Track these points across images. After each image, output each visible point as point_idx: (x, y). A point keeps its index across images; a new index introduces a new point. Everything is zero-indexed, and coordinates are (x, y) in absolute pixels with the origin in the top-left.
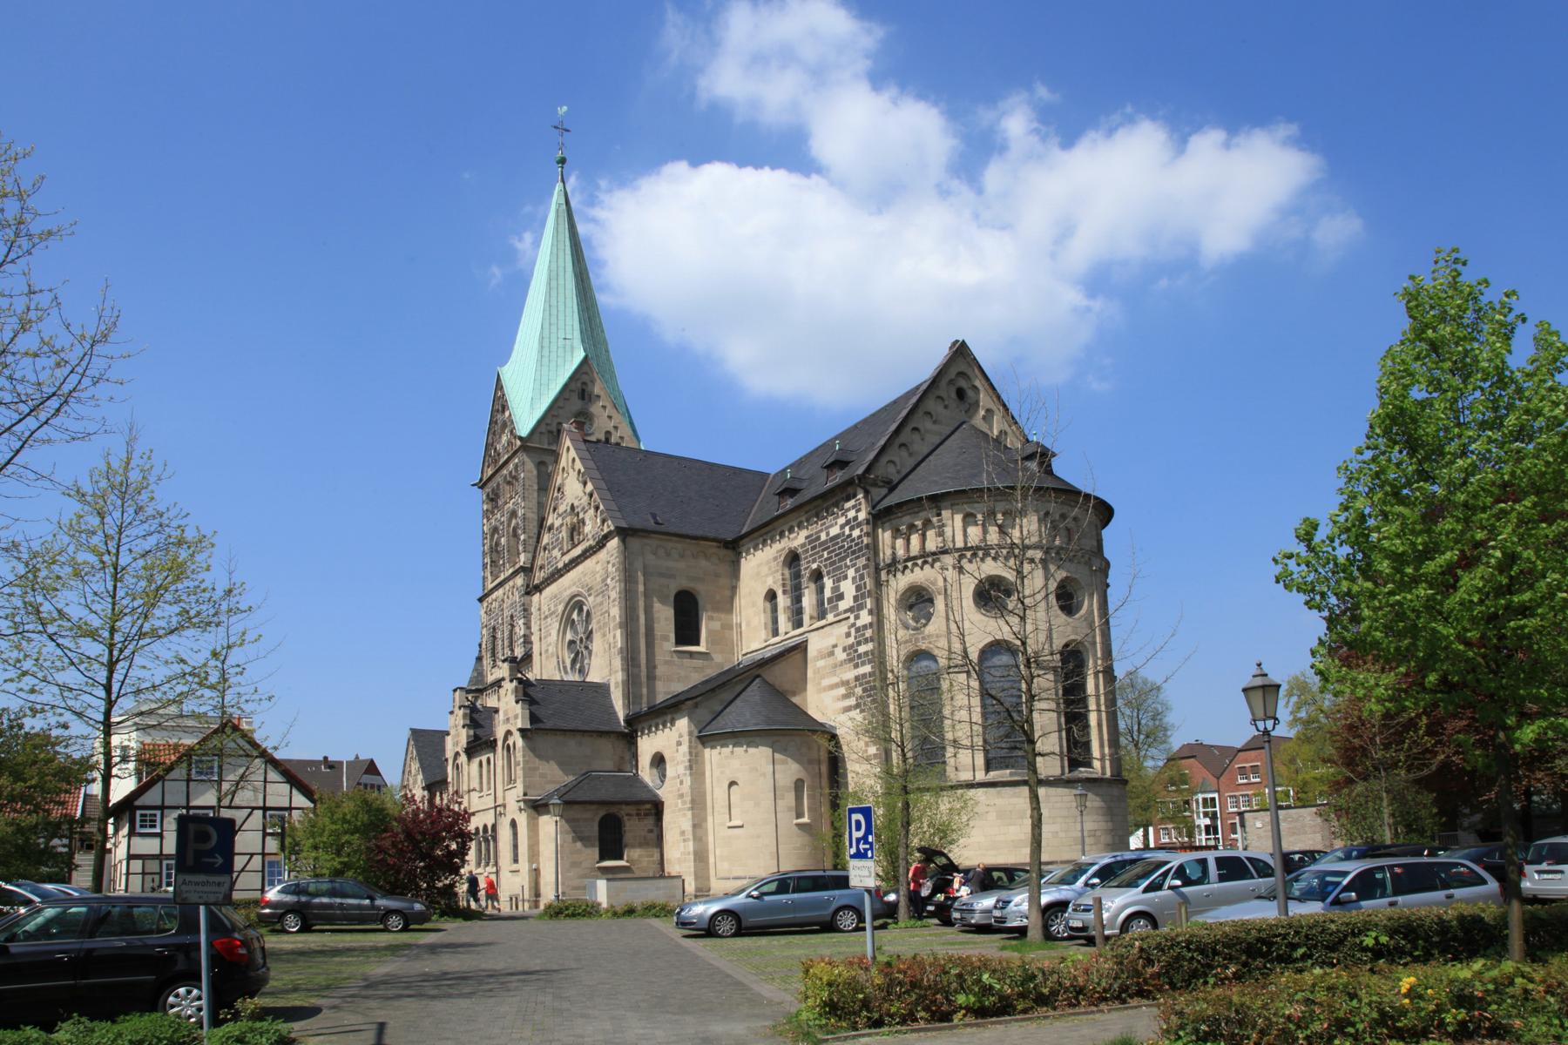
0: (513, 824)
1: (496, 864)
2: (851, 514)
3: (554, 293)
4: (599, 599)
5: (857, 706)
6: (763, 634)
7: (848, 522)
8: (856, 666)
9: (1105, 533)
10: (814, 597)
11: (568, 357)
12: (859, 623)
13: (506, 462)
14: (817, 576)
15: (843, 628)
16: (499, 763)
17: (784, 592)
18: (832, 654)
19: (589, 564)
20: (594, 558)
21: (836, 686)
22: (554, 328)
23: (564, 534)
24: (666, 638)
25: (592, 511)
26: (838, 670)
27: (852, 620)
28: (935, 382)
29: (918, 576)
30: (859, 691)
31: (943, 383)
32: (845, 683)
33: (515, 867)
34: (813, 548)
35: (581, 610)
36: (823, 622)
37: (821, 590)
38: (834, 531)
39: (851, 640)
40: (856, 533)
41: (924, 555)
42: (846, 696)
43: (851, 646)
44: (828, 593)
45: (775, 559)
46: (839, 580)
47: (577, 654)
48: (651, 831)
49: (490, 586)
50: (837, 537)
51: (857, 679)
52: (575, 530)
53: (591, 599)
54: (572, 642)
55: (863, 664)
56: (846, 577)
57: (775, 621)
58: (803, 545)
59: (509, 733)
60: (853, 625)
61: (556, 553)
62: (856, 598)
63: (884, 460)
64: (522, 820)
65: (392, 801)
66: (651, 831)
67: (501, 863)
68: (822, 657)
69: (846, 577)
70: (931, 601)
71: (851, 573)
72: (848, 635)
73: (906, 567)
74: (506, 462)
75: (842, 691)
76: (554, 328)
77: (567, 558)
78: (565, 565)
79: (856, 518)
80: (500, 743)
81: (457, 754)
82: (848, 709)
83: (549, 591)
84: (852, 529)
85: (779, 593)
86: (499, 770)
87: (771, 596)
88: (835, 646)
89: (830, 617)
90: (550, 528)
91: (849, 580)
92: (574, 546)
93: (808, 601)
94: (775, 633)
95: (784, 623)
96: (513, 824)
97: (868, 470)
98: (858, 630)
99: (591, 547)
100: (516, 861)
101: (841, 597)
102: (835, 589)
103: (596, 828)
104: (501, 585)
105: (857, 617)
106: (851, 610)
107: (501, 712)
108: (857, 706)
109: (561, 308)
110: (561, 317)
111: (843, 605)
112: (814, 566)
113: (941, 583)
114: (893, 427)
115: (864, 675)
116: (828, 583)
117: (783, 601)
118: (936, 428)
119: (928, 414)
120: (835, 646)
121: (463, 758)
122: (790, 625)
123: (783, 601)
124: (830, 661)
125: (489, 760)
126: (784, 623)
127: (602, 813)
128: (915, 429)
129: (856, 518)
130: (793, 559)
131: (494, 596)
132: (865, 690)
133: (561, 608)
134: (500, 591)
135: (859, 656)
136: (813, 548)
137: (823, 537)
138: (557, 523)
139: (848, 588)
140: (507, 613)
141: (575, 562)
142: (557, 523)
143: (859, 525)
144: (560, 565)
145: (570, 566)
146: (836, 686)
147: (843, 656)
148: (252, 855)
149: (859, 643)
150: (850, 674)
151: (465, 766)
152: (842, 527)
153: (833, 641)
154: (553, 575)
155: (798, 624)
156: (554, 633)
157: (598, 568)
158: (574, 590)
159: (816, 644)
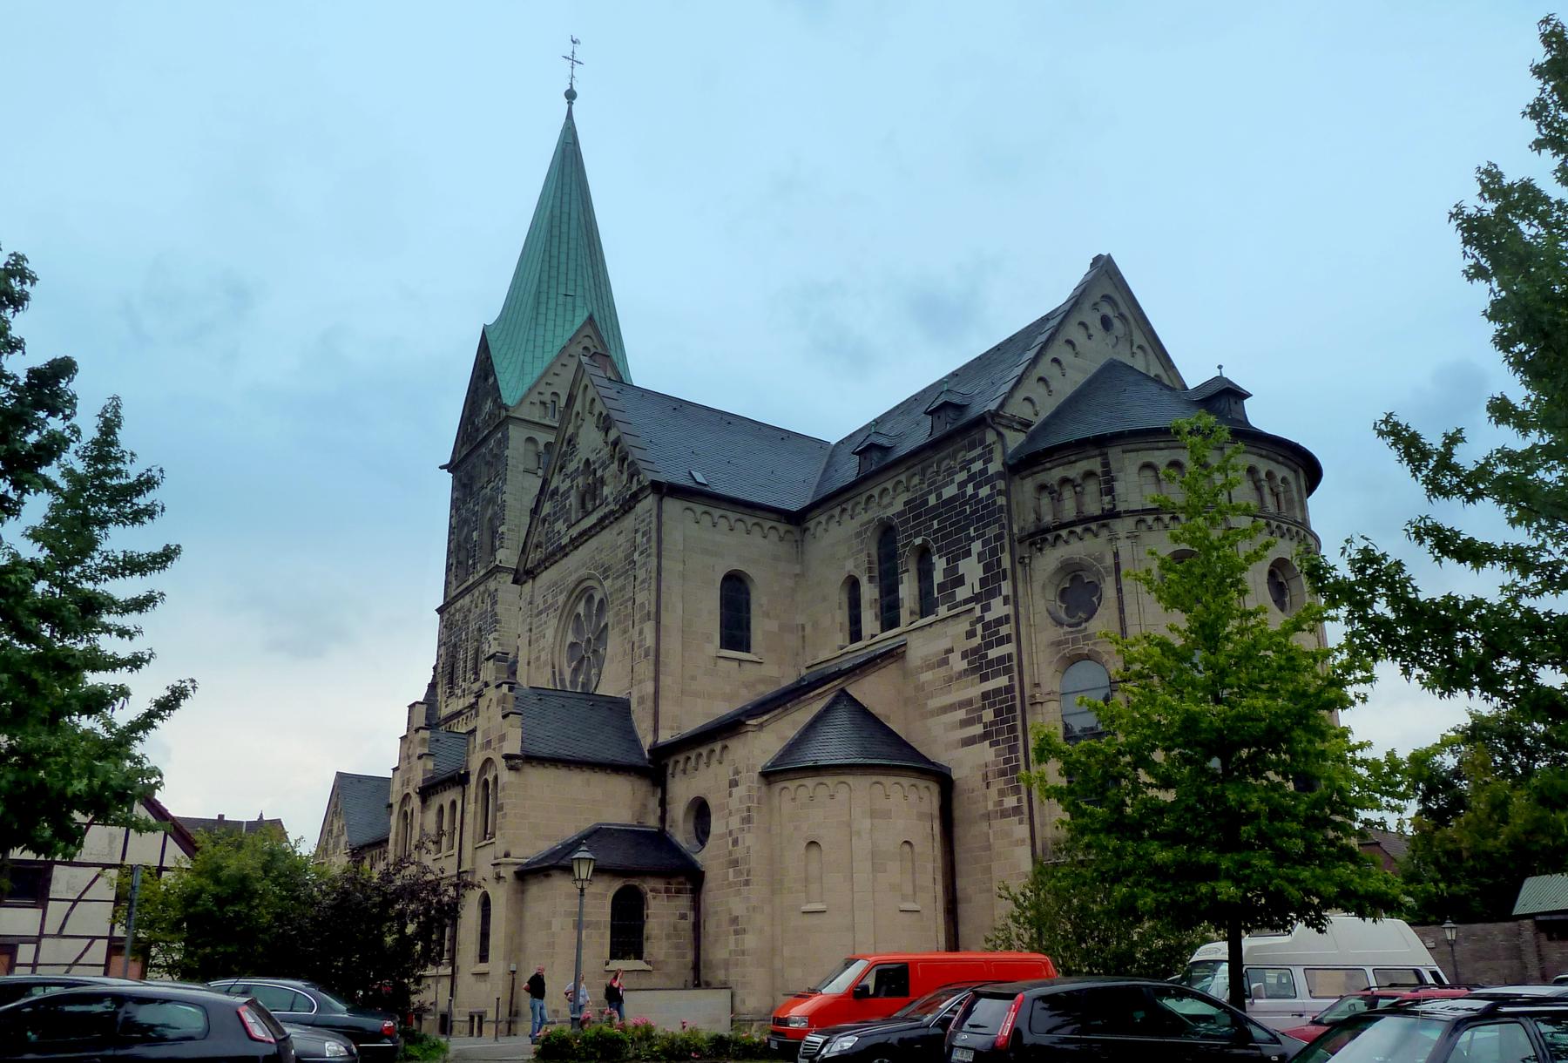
0: (486, 902)
1: (452, 962)
2: (977, 466)
3: (555, 241)
4: (620, 582)
5: (985, 736)
6: (841, 638)
7: (971, 478)
8: (984, 678)
9: (1313, 501)
10: (915, 584)
11: (569, 317)
12: (989, 617)
13: (485, 439)
14: (924, 554)
15: (963, 625)
16: (471, 808)
17: (871, 579)
18: (945, 662)
19: (607, 536)
20: (616, 528)
21: (952, 707)
22: (553, 283)
23: (573, 500)
24: (709, 639)
25: (615, 466)
26: (954, 686)
27: (978, 612)
28: (1076, 302)
29: (1077, 549)
30: (988, 715)
31: (1087, 305)
32: (967, 703)
33: (482, 967)
34: (916, 518)
35: (590, 599)
36: (931, 618)
37: (925, 574)
38: (949, 492)
39: (977, 641)
40: (984, 491)
41: (1083, 520)
42: (965, 723)
43: (975, 651)
44: (938, 577)
45: (858, 534)
46: (956, 559)
47: (581, 662)
48: (683, 917)
49: (454, 594)
50: (953, 499)
51: (985, 696)
52: (590, 494)
53: (607, 583)
54: (573, 645)
55: (996, 674)
56: (968, 554)
57: (855, 621)
58: (900, 514)
59: (488, 762)
60: (981, 619)
61: (560, 526)
62: (983, 582)
63: (1020, 394)
64: (500, 899)
65: (299, 867)
66: (683, 917)
67: (459, 960)
68: (930, 667)
69: (968, 554)
70: (1095, 588)
71: (977, 547)
72: (971, 634)
73: (1058, 537)
74: (485, 439)
75: (961, 714)
76: (553, 283)
77: (574, 532)
78: (572, 540)
79: (984, 471)
80: (473, 779)
81: (407, 797)
82: (969, 742)
83: (546, 577)
84: (977, 487)
85: (864, 581)
86: (469, 818)
87: (853, 584)
88: (951, 651)
89: (943, 611)
90: (555, 492)
91: (974, 556)
92: (587, 514)
93: (908, 590)
94: (856, 635)
95: (869, 622)
96: (486, 902)
97: (1002, 406)
98: (986, 627)
99: (612, 512)
100: (484, 957)
101: (960, 581)
102: (951, 570)
103: (608, 910)
104: (468, 590)
105: (986, 608)
106: (975, 598)
107: (479, 734)
108: (985, 736)
109: (563, 258)
110: (563, 268)
111: (962, 593)
112: (918, 541)
113: (1109, 561)
114: (1031, 354)
115: (997, 691)
116: (940, 564)
117: (869, 592)
118: (1078, 361)
119: (1069, 342)
120: (951, 651)
121: (416, 801)
122: (878, 624)
123: (869, 592)
124: (942, 672)
125: (453, 804)
126: (869, 622)
127: (617, 885)
128: (1055, 360)
129: (984, 471)
130: (887, 533)
131: (458, 605)
132: (998, 713)
133: (561, 599)
134: (467, 598)
135: (990, 663)
136: (919, 516)
137: (932, 500)
138: (563, 487)
139: (971, 569)
140: (473, 626)
141: (586, 535)
142: (563, 487)
143: (989, 480)
144: (565, 541)
145: (576, 543)
146: (952, 707)
147: (964, 665)
148: (94, 938)
149: (989, 646)
150: (975, 690)
151: (417, 814)
152: (962, 485)
153: (945, 644)
154: (553, 554)
155: (889, 619)
156: (550, 633)
157: (621, 539)
158: (583, 572)
159: (921, 648)
